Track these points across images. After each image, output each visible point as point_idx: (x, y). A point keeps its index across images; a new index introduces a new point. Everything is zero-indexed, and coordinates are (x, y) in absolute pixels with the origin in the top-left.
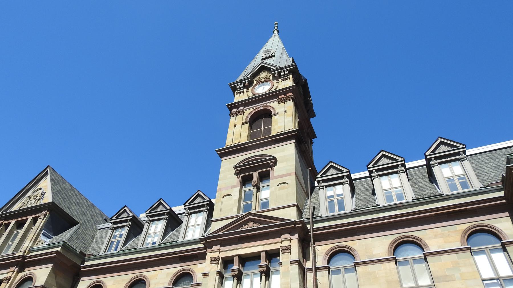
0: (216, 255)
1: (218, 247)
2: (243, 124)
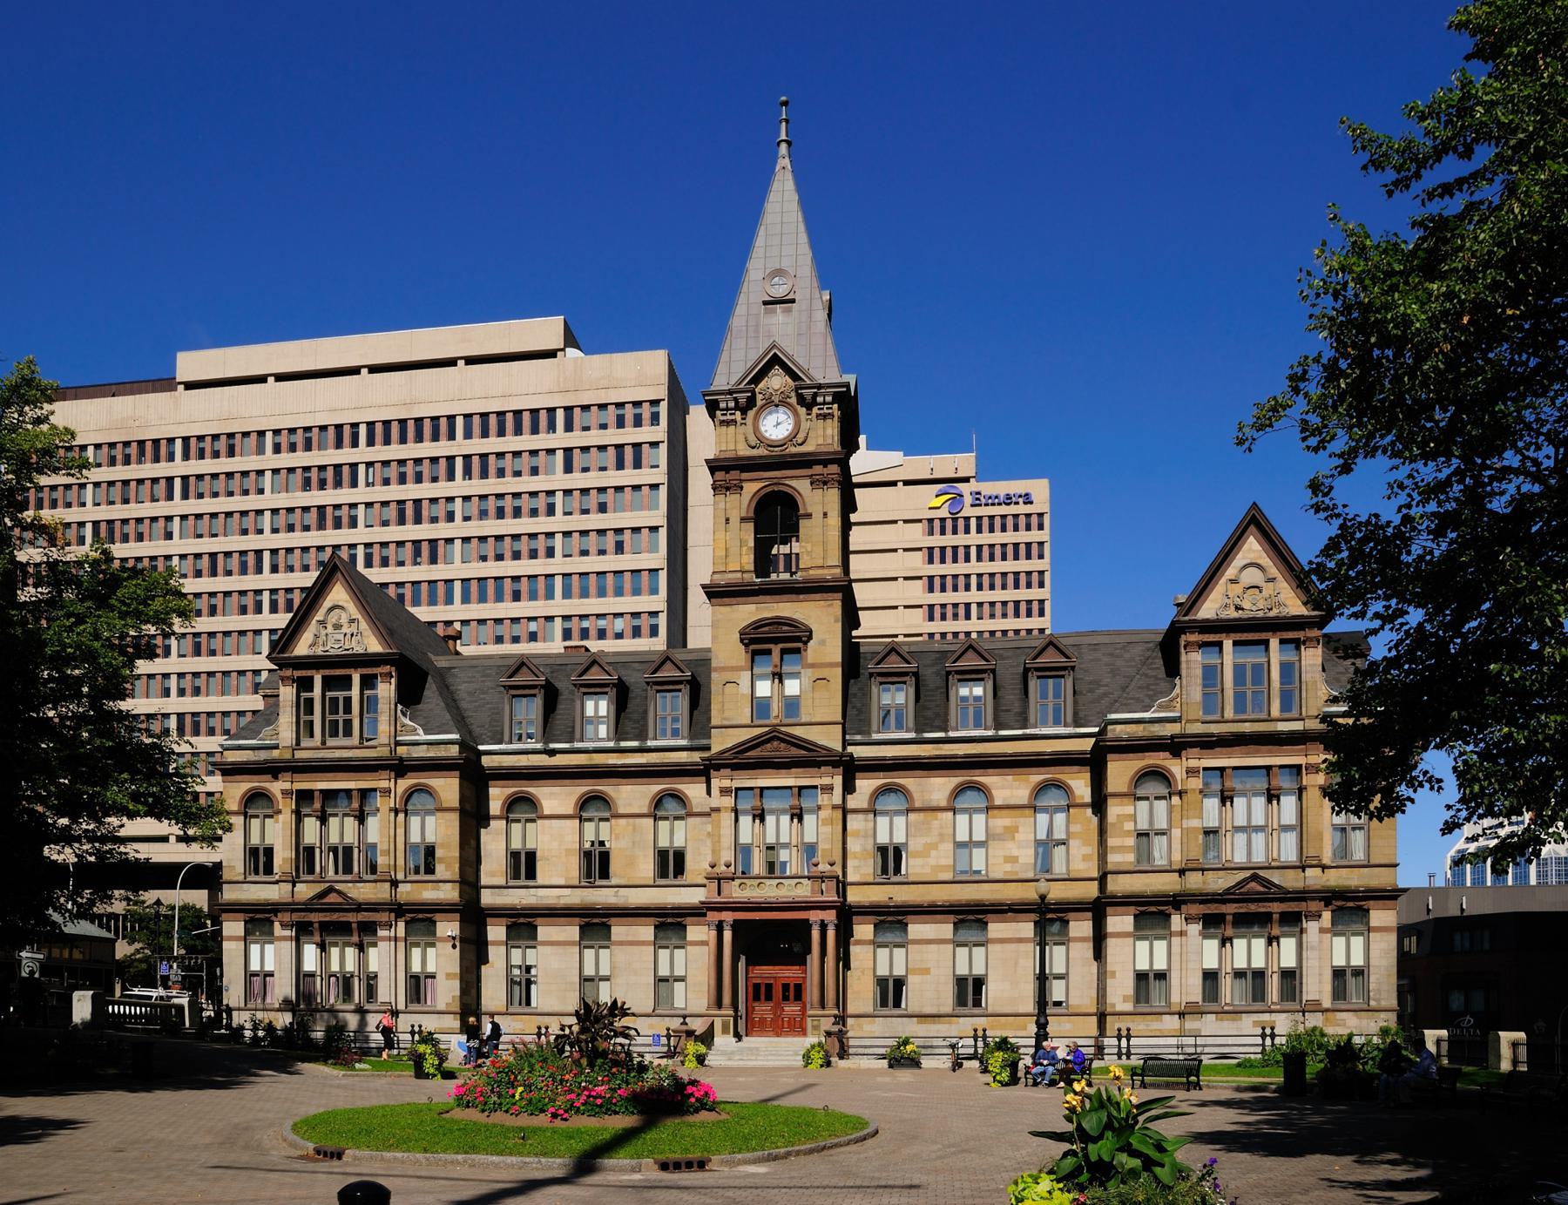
0: (726, 783)
1: (727, 771)
2: (743, 520)
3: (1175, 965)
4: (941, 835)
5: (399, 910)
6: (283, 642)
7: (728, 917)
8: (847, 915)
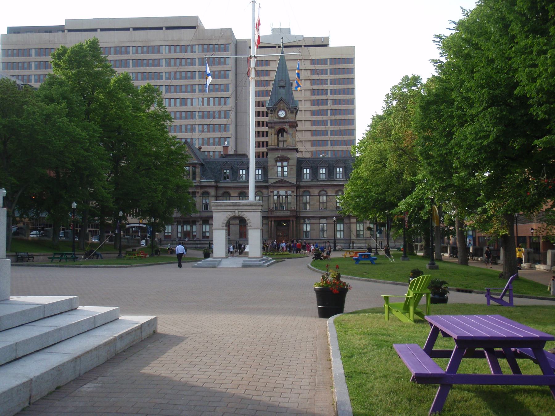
5: (201, 218)
7: (273, 219)
8: (297, 218)
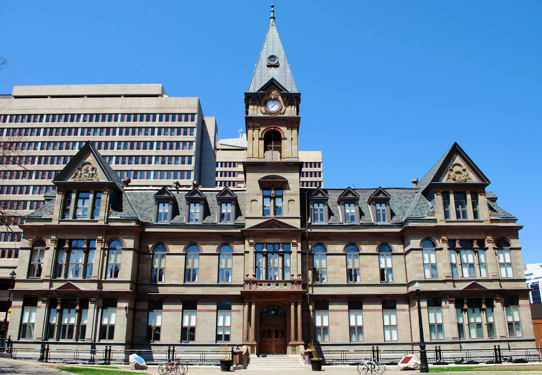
3: (496, 321)
4: (341, 265)
6: (60, 176)
